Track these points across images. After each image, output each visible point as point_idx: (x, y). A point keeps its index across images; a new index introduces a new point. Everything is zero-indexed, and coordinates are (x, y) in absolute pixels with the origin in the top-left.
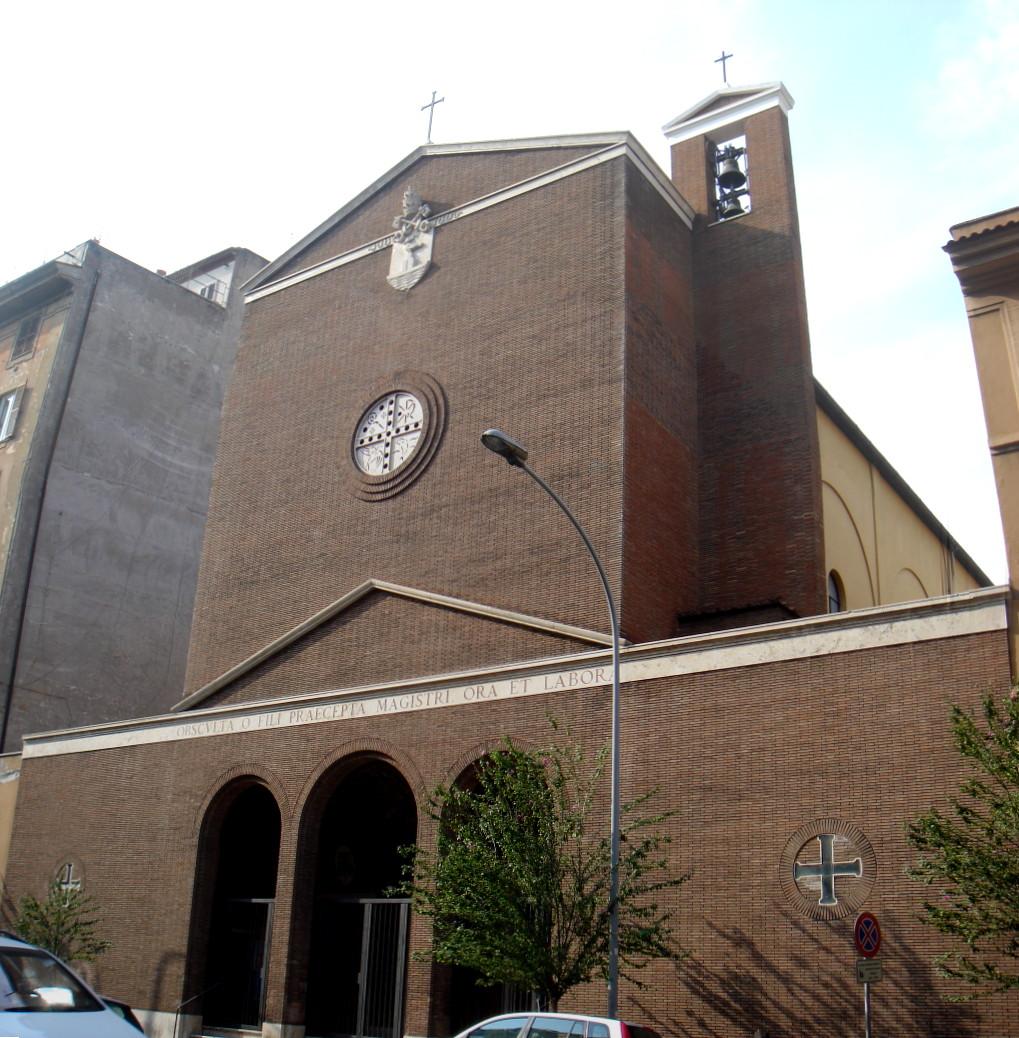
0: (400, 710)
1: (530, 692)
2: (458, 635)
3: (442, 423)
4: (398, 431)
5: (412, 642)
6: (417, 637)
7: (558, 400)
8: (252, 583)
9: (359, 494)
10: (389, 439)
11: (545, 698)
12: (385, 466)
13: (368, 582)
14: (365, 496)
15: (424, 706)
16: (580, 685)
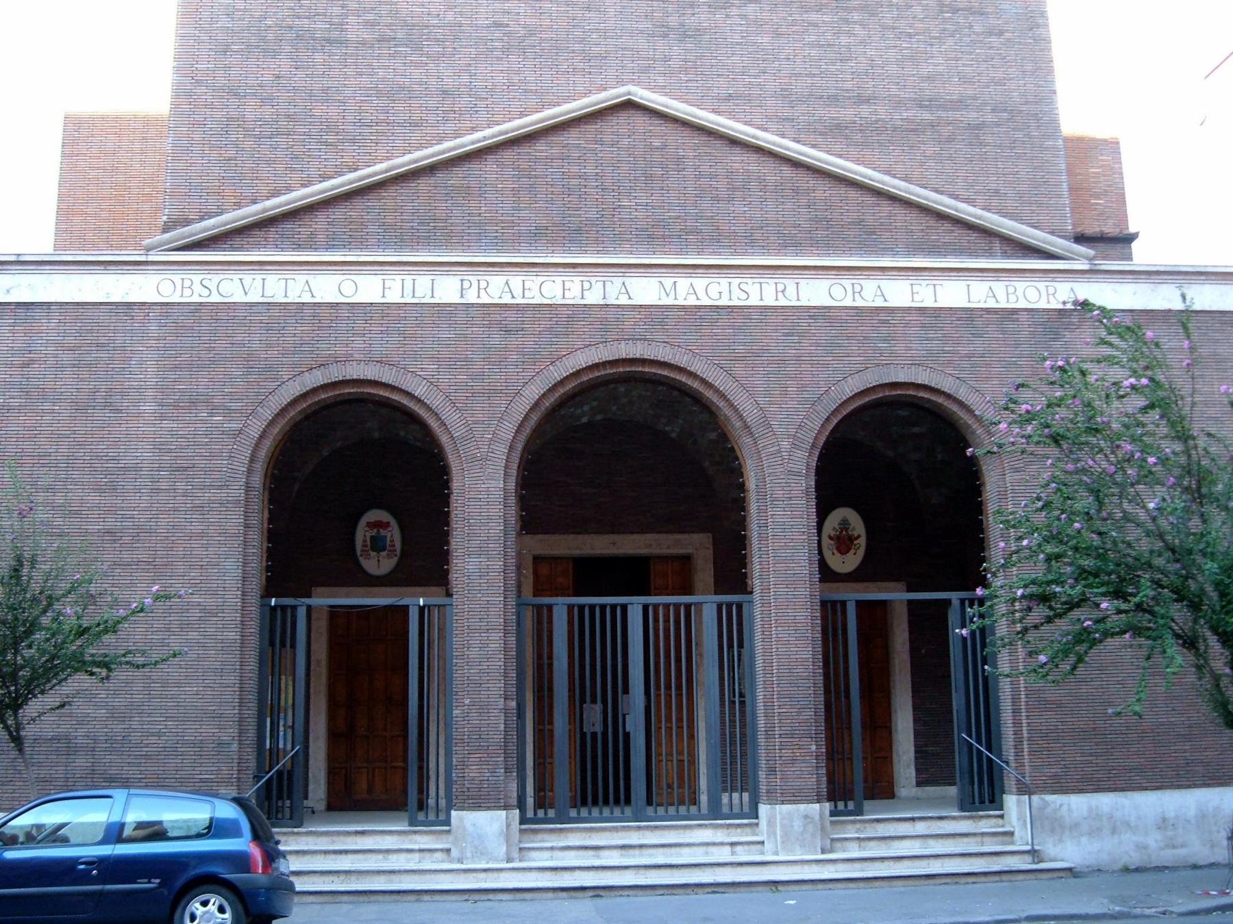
0: (705, 301)
1: (944, 302)
2: (804, 201)
5: (717, 199)
6: (724, 194)
8: (328, 40)
11: (968, 316)
13: (623, 90)
15: (754, 301)
16: (1022, 304)
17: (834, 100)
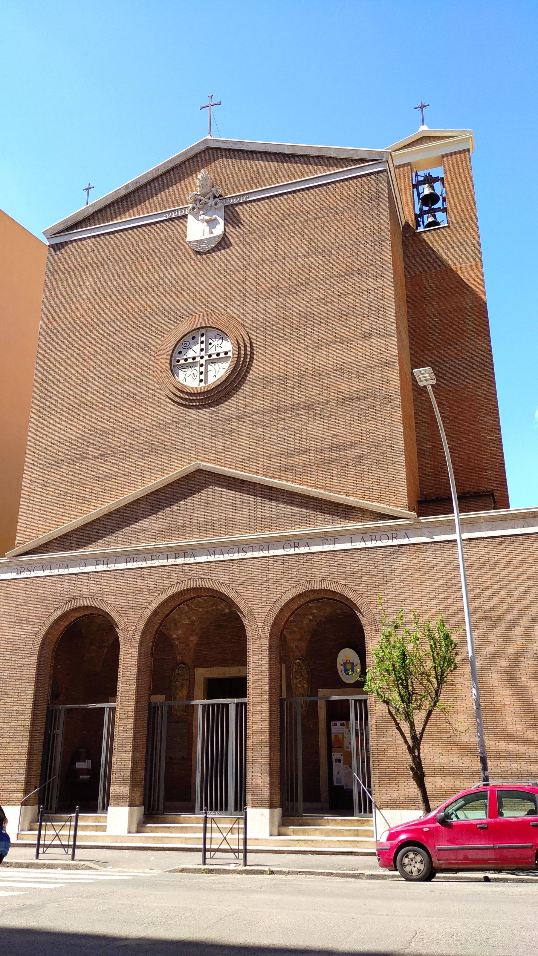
3: (249, 353)
4: (210, 356)
7: (345, 345)
9: (168, 392)
10: (203, 361)
12: (201, 381)
14: (172, 396)
17: (290, 455)
